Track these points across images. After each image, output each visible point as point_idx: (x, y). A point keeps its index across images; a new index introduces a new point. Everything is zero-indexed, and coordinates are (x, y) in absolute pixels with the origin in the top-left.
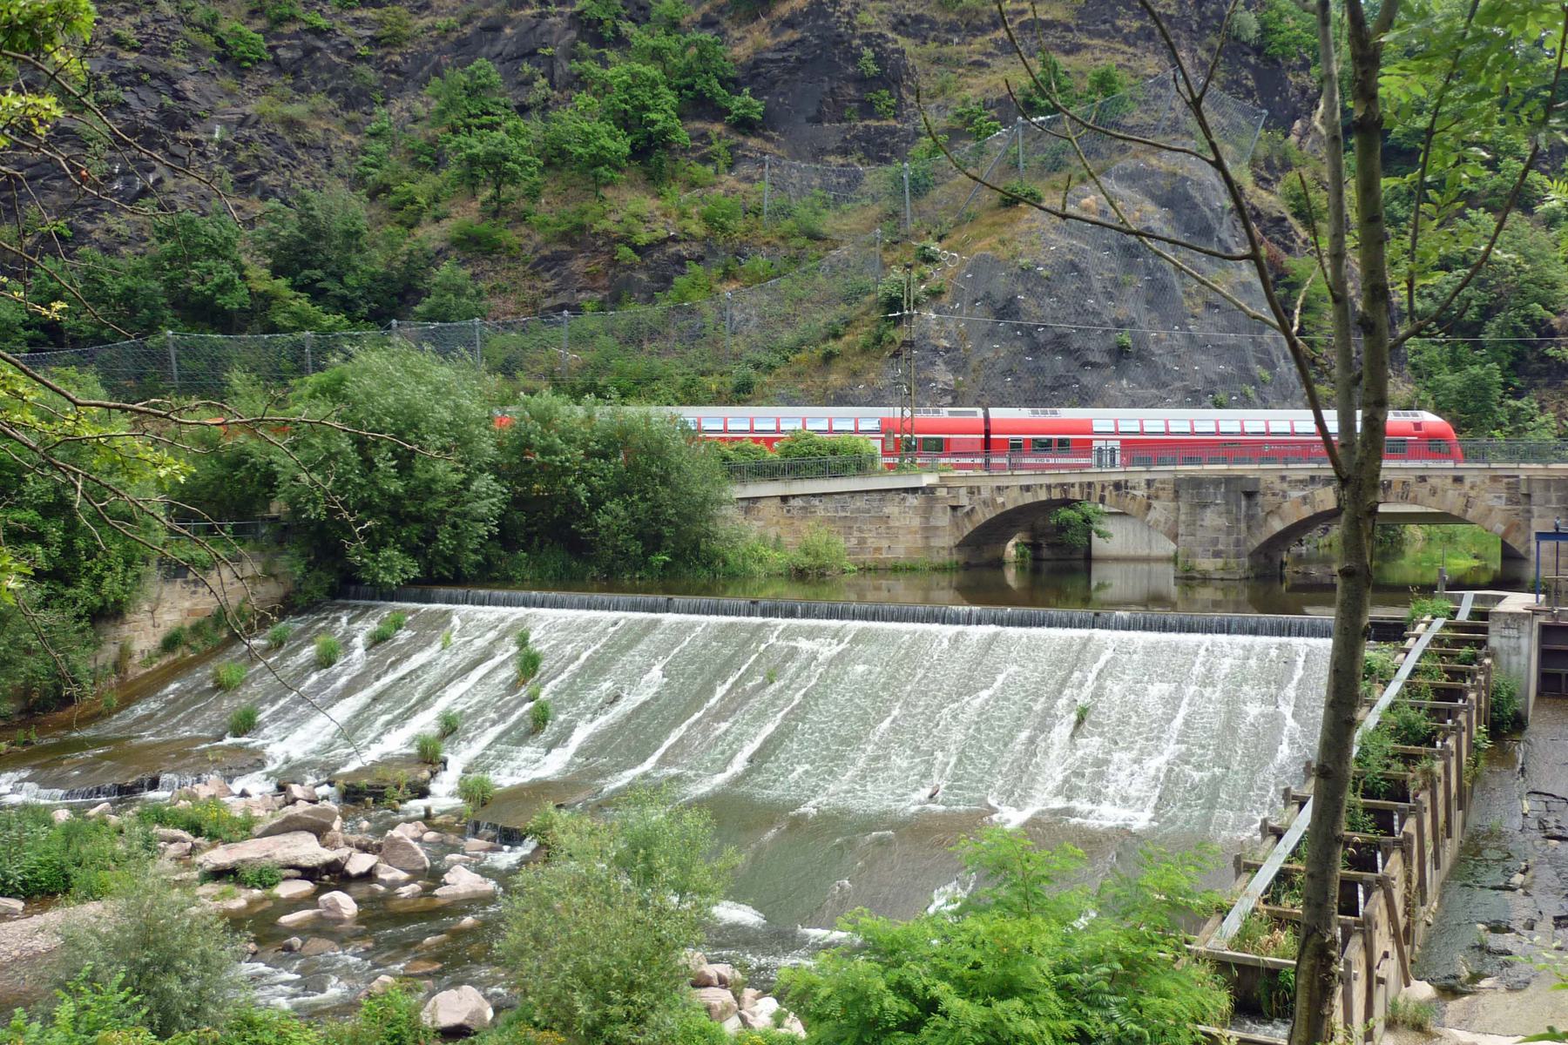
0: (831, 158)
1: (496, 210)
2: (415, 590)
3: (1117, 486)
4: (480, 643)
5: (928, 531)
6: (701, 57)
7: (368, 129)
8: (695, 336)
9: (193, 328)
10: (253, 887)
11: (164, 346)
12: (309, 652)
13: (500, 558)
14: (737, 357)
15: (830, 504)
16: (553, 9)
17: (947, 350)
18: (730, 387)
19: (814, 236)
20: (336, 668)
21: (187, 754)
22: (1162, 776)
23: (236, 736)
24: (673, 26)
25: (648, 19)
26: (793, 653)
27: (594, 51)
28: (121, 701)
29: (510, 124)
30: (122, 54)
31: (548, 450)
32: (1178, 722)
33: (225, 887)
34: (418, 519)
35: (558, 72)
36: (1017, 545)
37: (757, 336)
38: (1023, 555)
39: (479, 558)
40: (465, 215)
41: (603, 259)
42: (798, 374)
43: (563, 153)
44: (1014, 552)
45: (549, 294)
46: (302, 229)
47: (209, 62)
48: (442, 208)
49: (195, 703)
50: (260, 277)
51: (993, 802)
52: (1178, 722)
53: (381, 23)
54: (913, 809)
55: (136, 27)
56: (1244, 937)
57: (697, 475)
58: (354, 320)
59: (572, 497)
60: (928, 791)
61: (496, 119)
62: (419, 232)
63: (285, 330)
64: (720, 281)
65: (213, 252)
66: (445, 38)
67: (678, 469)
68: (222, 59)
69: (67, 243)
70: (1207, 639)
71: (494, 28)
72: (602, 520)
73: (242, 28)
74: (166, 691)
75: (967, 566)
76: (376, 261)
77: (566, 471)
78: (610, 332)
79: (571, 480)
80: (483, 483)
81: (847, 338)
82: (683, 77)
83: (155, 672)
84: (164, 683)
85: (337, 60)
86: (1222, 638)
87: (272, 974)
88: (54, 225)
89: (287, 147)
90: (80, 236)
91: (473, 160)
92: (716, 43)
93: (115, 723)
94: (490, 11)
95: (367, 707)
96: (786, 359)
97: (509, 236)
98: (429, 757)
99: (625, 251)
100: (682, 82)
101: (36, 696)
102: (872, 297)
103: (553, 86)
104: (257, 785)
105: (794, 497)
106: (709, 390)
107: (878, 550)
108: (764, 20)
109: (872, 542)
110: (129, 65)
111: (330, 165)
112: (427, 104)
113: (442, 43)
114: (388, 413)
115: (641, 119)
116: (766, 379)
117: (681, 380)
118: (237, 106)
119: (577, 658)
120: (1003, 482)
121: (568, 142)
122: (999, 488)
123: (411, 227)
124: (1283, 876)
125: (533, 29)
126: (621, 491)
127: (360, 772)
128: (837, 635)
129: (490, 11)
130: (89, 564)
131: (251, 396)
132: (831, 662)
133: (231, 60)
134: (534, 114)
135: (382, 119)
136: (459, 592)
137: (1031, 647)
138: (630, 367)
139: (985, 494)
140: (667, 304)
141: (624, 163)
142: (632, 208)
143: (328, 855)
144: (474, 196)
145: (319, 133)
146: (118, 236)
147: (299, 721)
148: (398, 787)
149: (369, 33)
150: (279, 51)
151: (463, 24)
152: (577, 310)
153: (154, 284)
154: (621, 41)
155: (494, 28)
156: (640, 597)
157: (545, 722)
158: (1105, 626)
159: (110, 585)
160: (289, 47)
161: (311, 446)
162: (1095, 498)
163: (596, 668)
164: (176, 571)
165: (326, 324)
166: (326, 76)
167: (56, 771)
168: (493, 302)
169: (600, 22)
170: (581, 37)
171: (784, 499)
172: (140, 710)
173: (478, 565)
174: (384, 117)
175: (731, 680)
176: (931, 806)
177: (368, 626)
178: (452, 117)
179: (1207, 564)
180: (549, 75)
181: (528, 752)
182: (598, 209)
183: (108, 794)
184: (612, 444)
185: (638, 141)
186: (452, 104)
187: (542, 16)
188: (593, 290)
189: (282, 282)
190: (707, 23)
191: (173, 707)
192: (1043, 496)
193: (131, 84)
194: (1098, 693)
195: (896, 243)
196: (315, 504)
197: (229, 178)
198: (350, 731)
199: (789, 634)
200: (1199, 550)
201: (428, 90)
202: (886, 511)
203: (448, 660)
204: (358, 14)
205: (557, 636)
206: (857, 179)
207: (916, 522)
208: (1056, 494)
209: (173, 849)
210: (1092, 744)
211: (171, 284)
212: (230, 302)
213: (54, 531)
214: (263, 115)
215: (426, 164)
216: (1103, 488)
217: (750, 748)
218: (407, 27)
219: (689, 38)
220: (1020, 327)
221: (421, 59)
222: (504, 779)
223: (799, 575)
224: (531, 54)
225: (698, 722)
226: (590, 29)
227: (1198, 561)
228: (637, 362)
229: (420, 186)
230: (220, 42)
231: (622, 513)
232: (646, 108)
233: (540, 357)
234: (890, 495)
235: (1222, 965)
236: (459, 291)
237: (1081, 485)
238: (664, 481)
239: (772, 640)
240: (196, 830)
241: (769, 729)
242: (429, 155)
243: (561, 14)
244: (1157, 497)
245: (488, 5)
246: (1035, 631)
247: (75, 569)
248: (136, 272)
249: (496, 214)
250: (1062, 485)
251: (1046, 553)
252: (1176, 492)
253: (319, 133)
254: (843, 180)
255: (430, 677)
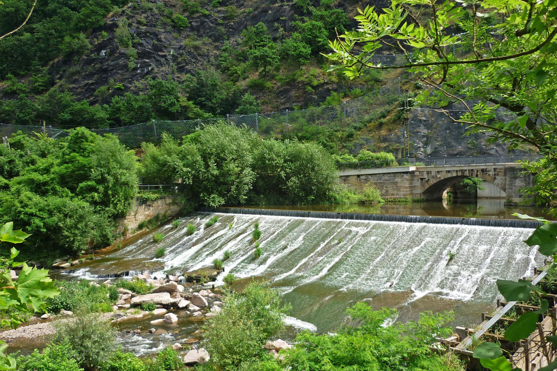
0: (384, 52)
1: (264, 75)
2: (224, 208)
3: (483, 170)
4: (243, 227)
5: (412, 187)
6: (337, 18)
7: (222, 48)
8: (333, 118)
9: (162, 119)
10: (146, 310)
11: (152, 125)
12: (185, 230)
13: (255, 197)
14: (348, 125)
15: (376, 178)
16: (286, 3)
17: (425, 121)
18: (345, 136)
19: (377, 81)
20: (193, 235)
21: (140, 264)
22: (479, 280)
23: (157, 258)
24: (328, 7)
25: (319, 5)
26: (350, 231)
27: (300, 18)
28: (123, 246)
29: (270, 44)
30: (141, 27)
31: (271, 159)
32: (488, 261)
33: (136, 310)
34: (225, 184)
35: (287, 25)
36: (448, 193)
37: (356, 117)
38: (450, 196)
39: (246, 197)
40: (254, 77)
41: (301, 91)
42: (370, 131)
43: (288, 54)
44: (446, 195)
45: (282, 104)
46: (198, 84)
47: (169, 28)
48: (246, 75)
49: (146, 246)
50: (183, 100)
51: (413, 289)
52: (488, 261)
53: (227, 12)
54: (382, 290)
55: (145, 18)
56: (474, 345)
57: (325, 168)
58: (215, 115)
59: (279, 175)
60: (389, 284)
61: (265, 43)
62: (238, 84)
63: (193, 119)
64: (343, 98)
65: (169, 93)
66: (248, 16)
67: (318, 165)
68: (174, 27)
69: (119, 92)
70: (505, 229)
71: (265, 11)
72: (290, 184)
73: (180, 16)
74: (138, 242)
75: (427, 201)
76: (224, 94)
77: (278, 167)
78: (304, 117)
79: (279, 170)
80: (248, 170)
81: (388, 117)
82: (331, 25)
83: (136, 236)
84: (138, 240)
85: (212, 25)
86: (511, 229)
87: (143, 341)
88: (119, 85)
89: (195, 56)
90: (127, 89)
91: (256, 58)
92: (342, 12)
93: (118, 254)
94: (264, 5)
95: (201, 249)
96: (366, 125)
97: (269, 84)
98: (218, 267)
99: (309, 88)
100: (330, 27)
101: (95, 243)
102: (397, 102)
103: (285, 30)
104: (160, 275)
105: (362, 175)
106: (338, 137)
107: (393, 194)
108: (360, 3)
109: (391, 192)
110: (143, 31)
111: (209, 61)
112: (242, 39)
113: (248, 17)
114: (214, 147)
115: (315, 41)
116: (358, 133)
117: (328, 133)
118: (178, 43)
119: (274, 233)
120: (439, 169)
121: (289, 50)
122: (438, 172)
123: (236, 81)
124: (500, 323)
125: (278, 11)
126: (296, 173)
127: (194, 272)
128: (367, 226)
129: (264, 5)
130: (113, 199)
131: (169, 142)
132: (364, 236)
133: (177, 27)
134: (278, 41)
135: (227, 44)
136: (238, 209)
137: (437, 232)
138: (310, 130)
139: (433, 174)
140: (324, 106)
141: (309, 57)
142: (311, 72)
143: (172, 300)
144: (257, 70)
145: (205, 51)
146: (139, 88)
147: (178, 253)
148: (205, 277)
149: (223, 15)
150: (193, 23)
151: (254, 11)
152: (292, 109)
153: (149, 104)
154: (309, 14)
155: (265, 11)
156: (299, 211)
157: (259, 256)
158: (467, 223)
159: (120, 207)
160: (196, 22)
161: (187, 159)
162: (474, 175)
163: (282, 235)
164: (143, 202)
165: (206, 116)
166: (208, 31)
167: (97, 269)
168: (262, 107)
169: (302, 7)
170: (295, 13)
171: (358, 176)
172: (129, 249)
173: (246, 200)
174: (227, 44)
175: (326, 242)
176: (390, 290)
177: (206, 220)
178: (250, 43)
179: (516, 200)
180: (284, 27)
181: (252, 266)
182: (299, 73)
183: (111, 277)
184: (294, 158)
185: (314, 48)
186: (250, 39)
187: (282, 6)
188: (298, 102)
189: (191, 102)
190: (340, 5)
191: (140, 248)
192: (454, 174)
193: (144, 37)
194: (460, 247)
195: (407, 82)
196: (189, 179)
197: (175, 67)
198: (195, 257)
199: (349, 225)
200: (514, 195)
201: (242, 34)
202: (396, 180)
203: (231, 233)
204: (219, 9)
205: (268, 226)
206: (394, 59)
207: (407, 185)
208: (460, 174)
209: (125, 296)
210: (454, 268)
211: (155, 104)
212: (173, 109)
213: (101, 188)
214: (187, 45)
215: (241, 60)
216: (477, 171)
217: (329, 266)
218: (235, 12)
219: (333, 11)
220: (452, 112)
221: (240, 24)
222: (242, 275)
223: (362, 203)
224: (278, 20)
225: (312, 257)
226: (298, 10)
227: (513, 199)
228: (312, 128)
229: (239, 67)
230: (173, 21)
231: (297, 181)
232: (317, 37)
233: (279, 126)
234: (397, 174)
235: (462, 356)
236: (251, 104)
237: (469, 170)
238: (313, 169)
239: (343, 227)
240: (133, 289)
241: (337, 259)
242: (243, 57)
243: (288, 5)
244: (498, 175)
245: (263, 3)
246: (439, 225)
247: (109, 201)
248: (143, 100)
249: (264, 76)
250: (462, 170)
251: (459, 195)
252: (505, 173)
253: (205, 51)
254: (388, 60)
255: (223, 240)
